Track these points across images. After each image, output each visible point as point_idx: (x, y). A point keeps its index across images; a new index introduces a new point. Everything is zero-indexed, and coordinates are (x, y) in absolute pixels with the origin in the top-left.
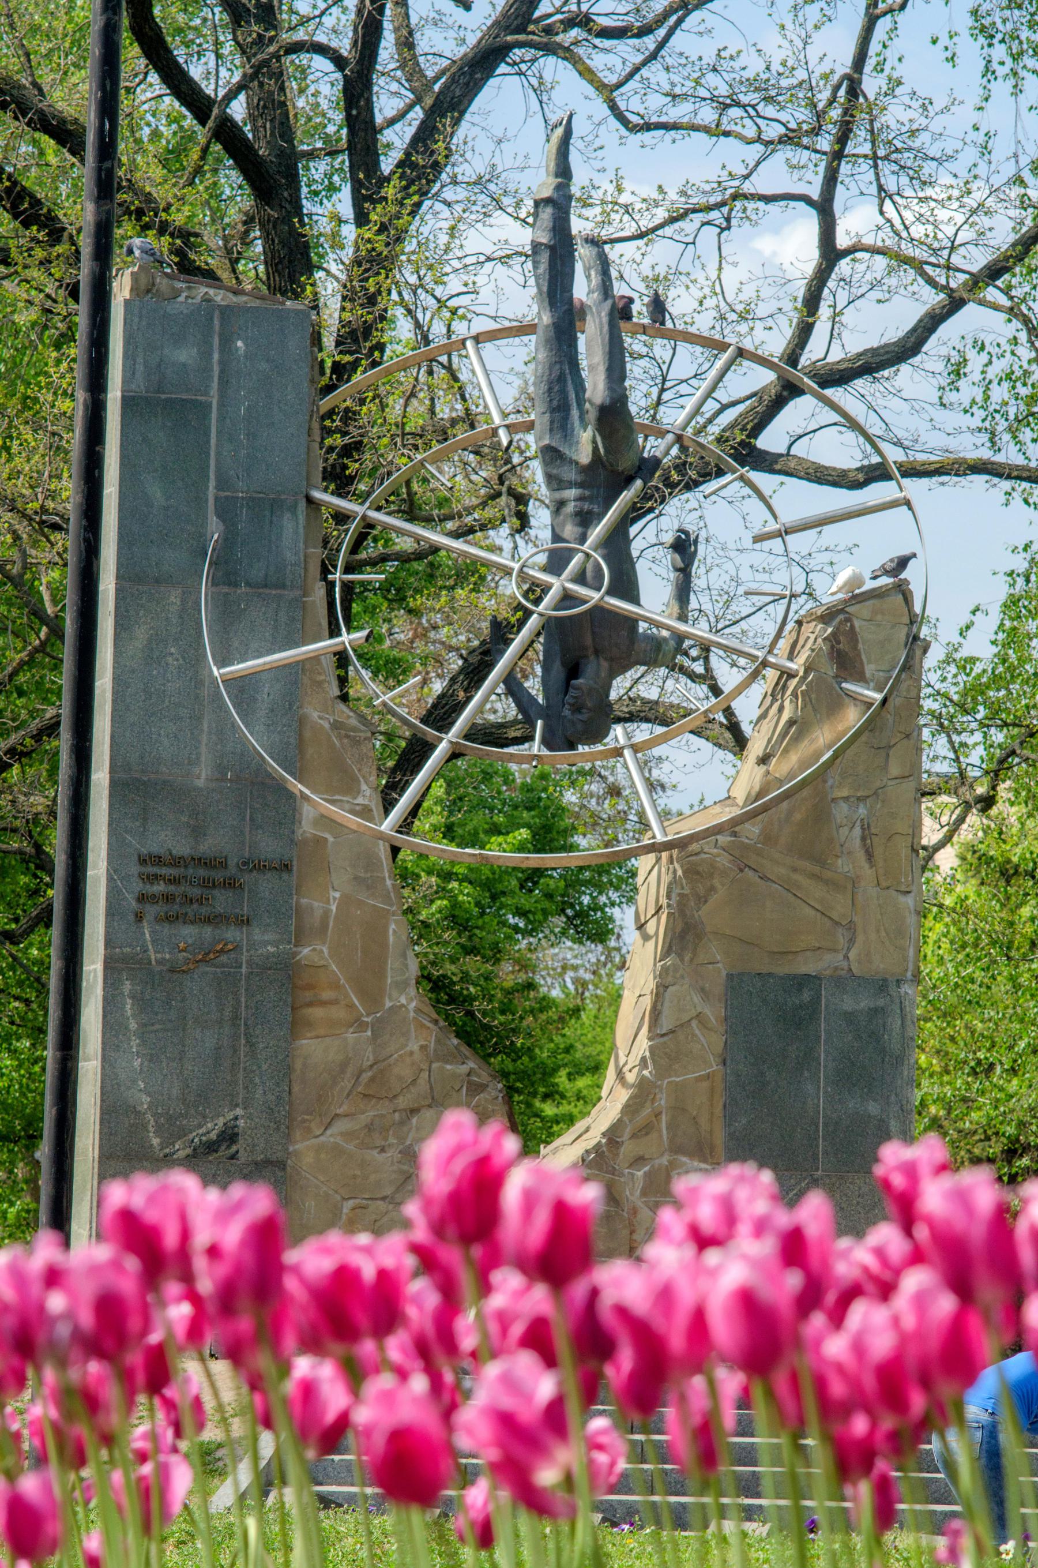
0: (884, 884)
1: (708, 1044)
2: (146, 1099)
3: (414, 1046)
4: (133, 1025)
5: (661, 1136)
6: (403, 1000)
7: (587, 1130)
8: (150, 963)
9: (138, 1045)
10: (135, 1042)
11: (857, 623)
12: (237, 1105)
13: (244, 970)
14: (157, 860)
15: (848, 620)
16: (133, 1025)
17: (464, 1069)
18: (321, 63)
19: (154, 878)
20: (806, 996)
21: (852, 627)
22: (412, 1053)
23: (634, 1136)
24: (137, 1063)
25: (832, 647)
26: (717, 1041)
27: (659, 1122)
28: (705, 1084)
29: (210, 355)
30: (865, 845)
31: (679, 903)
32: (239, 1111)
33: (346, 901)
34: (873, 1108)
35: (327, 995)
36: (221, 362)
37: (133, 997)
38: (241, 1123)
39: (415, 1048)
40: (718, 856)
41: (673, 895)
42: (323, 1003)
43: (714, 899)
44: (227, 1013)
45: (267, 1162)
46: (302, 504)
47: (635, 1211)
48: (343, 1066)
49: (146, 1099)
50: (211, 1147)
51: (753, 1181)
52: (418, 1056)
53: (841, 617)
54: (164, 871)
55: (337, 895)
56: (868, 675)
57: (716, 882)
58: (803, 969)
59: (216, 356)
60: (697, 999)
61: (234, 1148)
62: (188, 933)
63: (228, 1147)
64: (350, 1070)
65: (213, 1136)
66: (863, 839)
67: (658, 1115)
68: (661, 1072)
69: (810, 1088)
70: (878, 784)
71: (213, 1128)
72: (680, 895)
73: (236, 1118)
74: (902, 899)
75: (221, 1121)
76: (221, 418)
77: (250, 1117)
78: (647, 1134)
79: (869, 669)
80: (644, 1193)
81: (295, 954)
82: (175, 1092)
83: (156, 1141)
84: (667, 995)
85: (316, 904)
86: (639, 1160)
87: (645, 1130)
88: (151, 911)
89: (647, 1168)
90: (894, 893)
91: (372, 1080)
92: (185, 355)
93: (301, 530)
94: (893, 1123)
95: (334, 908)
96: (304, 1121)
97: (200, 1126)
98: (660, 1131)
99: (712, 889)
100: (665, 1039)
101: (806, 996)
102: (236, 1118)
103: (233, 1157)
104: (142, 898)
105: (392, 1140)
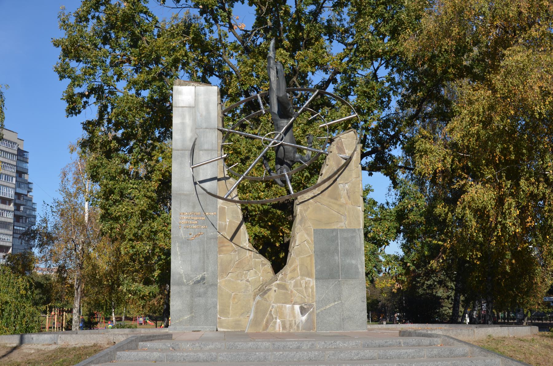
2: (182, 271)
4: (179, 253)
11: (343, 140)
16: (179, 253)
20: (334, 234)
23: (291, 272)
24: (180, 262)
32: (205, 273)
33: (230, 222)
34: (354, 262)
38: (206, 275)
42: (225, 246)
43: (309, 210)
44: (202, 249)
45: (212, 285)
47: (292, 292)
48: (231, 261)
49: (182, 271)
50: (198, 282)
51: (263, 265)
52: (249, 258)
57: (310, 206)
58: (334, 227)
60: (306, 236)
64: (233, 262)
65: (199, 279)
66: (347, 193)
69: (336, 258)
71: (199, 277)
74: (359, 208)
75: (201, 276)
77: (208, 274)
80: (294, 287)
82: (189, 269)
83: (185, 281)
86: (292, 278)
91: (238, 264)
99: (309, 208)
101: (334, 234)
105: (243, 278)
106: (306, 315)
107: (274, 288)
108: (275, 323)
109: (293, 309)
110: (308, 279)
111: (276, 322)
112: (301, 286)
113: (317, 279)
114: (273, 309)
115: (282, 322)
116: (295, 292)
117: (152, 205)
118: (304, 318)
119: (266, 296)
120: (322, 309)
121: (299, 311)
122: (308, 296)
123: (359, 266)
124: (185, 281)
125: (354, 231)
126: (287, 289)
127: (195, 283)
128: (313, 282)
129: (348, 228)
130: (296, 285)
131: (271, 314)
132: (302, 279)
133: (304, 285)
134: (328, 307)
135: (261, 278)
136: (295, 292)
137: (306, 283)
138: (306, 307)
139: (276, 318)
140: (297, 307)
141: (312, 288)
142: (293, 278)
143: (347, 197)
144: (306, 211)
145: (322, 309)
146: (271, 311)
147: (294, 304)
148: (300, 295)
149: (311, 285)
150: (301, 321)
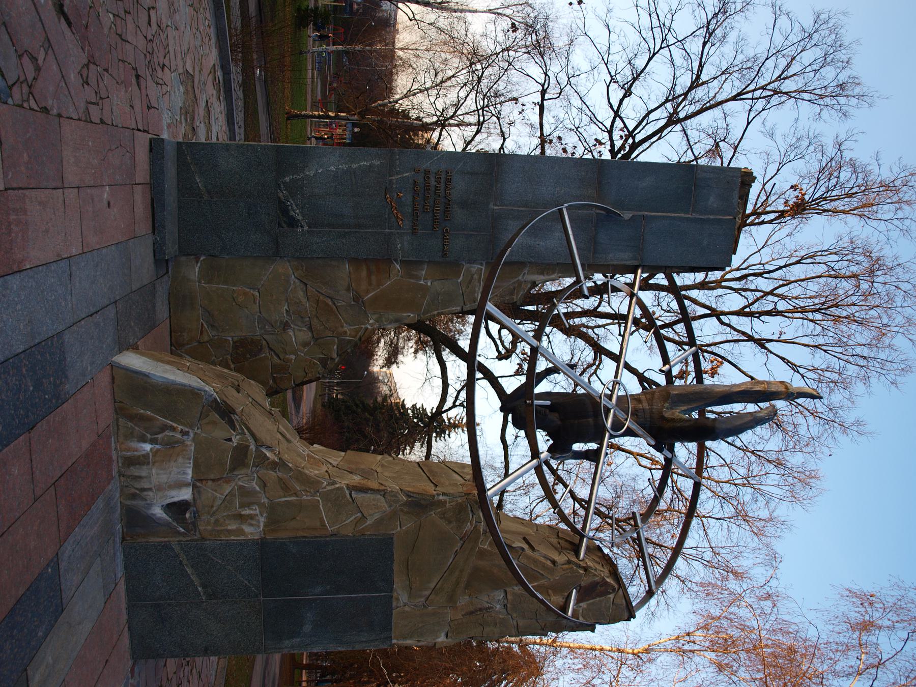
0: (452, 624)
1: (343, 525)
2: (312, 173)
3: (346, 328)
4: (354, 166)
5: (281, 497)
6: (371, 321)
7: (288, 441)
8: (390, 176)
9: (343, 169)
10: (345, 167)
11: (612, 596)
12: (310, 227)
13: (387, 230)
14: (448, 181)
15: (614, 590)
16: (354, 166)
17: (335, 356)
18: (596, 304)
19: (438, 180)
21: (610, 593)
22: (342, 326)
23: (280, 479)
24: (333, 168)
25: (598, 583)
26: (349, 532)
27: (290, 496)
28: (318, 524)
29: (712, 214)
30: (476, 611)
31: (440, 501)
32: (306, 228)
33: (424, 289)
34: (307, 628)
35: (373, 278)
36: (709, 220)
37: (370, 166)
38: (300, 230)
39: (346, 329)
40: (471, 524)
41: (445, 498)
46: (636, 263)
47: (228, 481)
49: (312, 173)
50: (285, 211)
52: (340, 330)
53: (616, 586)
54: (443, 185)
55: (429, 284)
56: (581, 604)
59: (711, 217)
60: (377, 516)
61: (284, 225)
62: (406, 197)
63: (285, 222)
65: (292, 213)
66: (480, 610)
67: (296, 494)
68: (326, 496)
69: (319, 589)
70: (514, 615)
71: (297, 214)
72: (445, 502)
73: (302, 227)
74: (443, 635)
75: (300, 218)
76: (680, 219)
78: (282, 488)
79: (584, 605)
80: (241, 487)
81: (396, 260)
83: (287, 179)
84: (379, 496)
85: (424, 272)
86: (264, 485)
87: (285, 488)
88: (420, 179)
89: (258, 488)
90: (446, 630)
91: (327, 304)
92: (713, 201)
93: (623, 263)
94: (298, 640)
95: (422, 282)
96: (302, 266)
97: (297, 206)
98: (285, 497)
99: (450, 522)
100: (348, 496)
102: (302, 227)
103: (280, 225)
104: (427, 172)
106: (164, 515)
107: (236, 440)
108: (143, 440)
109: (180, 485)
110: (262, 520)
111: (145, 441)
112: (242, 506)
113: (262, 544)
114: (179, 436)
115: (146, 456)
116: (227, 489)
117: (366, 660)
118: (158, 511)
119: (216, 416)
120: (183, 557)
121: (176, 499)
122: (217, 521)
123: (297, 640)
124: (287, 179)
125: (387, 626)
126: (233, 469)
127: (280, 202)
128: (252, 532)
129: (394, 612)
130: (244, 492)
131: (164, 428)
132: (262, 506)
133: (246, 512)
134: (189, 570)
135: (293, 357)
136: (227, 489)
137: (251, 517)
138: (188, 515)
139: (153, 441)
140: (186, 494)
141: (240, 532)
142: (265, 485)
143: (472, 609)
144: (443, 516)
145: (183, 557)
146: (174, 429)
147: (194, 487)
148: (218, 502)
149: (247, 529)
150: (150, 506)
